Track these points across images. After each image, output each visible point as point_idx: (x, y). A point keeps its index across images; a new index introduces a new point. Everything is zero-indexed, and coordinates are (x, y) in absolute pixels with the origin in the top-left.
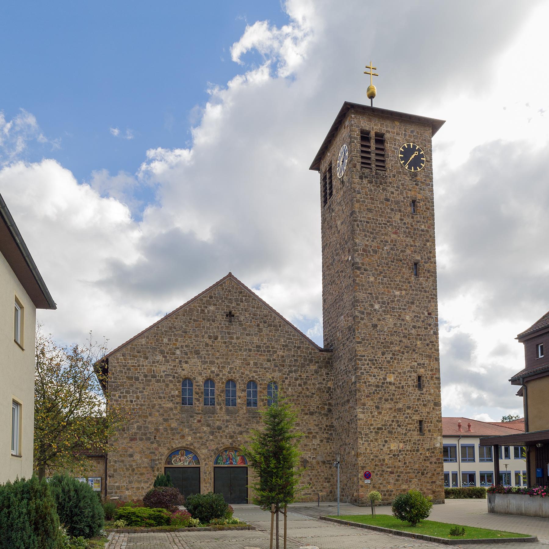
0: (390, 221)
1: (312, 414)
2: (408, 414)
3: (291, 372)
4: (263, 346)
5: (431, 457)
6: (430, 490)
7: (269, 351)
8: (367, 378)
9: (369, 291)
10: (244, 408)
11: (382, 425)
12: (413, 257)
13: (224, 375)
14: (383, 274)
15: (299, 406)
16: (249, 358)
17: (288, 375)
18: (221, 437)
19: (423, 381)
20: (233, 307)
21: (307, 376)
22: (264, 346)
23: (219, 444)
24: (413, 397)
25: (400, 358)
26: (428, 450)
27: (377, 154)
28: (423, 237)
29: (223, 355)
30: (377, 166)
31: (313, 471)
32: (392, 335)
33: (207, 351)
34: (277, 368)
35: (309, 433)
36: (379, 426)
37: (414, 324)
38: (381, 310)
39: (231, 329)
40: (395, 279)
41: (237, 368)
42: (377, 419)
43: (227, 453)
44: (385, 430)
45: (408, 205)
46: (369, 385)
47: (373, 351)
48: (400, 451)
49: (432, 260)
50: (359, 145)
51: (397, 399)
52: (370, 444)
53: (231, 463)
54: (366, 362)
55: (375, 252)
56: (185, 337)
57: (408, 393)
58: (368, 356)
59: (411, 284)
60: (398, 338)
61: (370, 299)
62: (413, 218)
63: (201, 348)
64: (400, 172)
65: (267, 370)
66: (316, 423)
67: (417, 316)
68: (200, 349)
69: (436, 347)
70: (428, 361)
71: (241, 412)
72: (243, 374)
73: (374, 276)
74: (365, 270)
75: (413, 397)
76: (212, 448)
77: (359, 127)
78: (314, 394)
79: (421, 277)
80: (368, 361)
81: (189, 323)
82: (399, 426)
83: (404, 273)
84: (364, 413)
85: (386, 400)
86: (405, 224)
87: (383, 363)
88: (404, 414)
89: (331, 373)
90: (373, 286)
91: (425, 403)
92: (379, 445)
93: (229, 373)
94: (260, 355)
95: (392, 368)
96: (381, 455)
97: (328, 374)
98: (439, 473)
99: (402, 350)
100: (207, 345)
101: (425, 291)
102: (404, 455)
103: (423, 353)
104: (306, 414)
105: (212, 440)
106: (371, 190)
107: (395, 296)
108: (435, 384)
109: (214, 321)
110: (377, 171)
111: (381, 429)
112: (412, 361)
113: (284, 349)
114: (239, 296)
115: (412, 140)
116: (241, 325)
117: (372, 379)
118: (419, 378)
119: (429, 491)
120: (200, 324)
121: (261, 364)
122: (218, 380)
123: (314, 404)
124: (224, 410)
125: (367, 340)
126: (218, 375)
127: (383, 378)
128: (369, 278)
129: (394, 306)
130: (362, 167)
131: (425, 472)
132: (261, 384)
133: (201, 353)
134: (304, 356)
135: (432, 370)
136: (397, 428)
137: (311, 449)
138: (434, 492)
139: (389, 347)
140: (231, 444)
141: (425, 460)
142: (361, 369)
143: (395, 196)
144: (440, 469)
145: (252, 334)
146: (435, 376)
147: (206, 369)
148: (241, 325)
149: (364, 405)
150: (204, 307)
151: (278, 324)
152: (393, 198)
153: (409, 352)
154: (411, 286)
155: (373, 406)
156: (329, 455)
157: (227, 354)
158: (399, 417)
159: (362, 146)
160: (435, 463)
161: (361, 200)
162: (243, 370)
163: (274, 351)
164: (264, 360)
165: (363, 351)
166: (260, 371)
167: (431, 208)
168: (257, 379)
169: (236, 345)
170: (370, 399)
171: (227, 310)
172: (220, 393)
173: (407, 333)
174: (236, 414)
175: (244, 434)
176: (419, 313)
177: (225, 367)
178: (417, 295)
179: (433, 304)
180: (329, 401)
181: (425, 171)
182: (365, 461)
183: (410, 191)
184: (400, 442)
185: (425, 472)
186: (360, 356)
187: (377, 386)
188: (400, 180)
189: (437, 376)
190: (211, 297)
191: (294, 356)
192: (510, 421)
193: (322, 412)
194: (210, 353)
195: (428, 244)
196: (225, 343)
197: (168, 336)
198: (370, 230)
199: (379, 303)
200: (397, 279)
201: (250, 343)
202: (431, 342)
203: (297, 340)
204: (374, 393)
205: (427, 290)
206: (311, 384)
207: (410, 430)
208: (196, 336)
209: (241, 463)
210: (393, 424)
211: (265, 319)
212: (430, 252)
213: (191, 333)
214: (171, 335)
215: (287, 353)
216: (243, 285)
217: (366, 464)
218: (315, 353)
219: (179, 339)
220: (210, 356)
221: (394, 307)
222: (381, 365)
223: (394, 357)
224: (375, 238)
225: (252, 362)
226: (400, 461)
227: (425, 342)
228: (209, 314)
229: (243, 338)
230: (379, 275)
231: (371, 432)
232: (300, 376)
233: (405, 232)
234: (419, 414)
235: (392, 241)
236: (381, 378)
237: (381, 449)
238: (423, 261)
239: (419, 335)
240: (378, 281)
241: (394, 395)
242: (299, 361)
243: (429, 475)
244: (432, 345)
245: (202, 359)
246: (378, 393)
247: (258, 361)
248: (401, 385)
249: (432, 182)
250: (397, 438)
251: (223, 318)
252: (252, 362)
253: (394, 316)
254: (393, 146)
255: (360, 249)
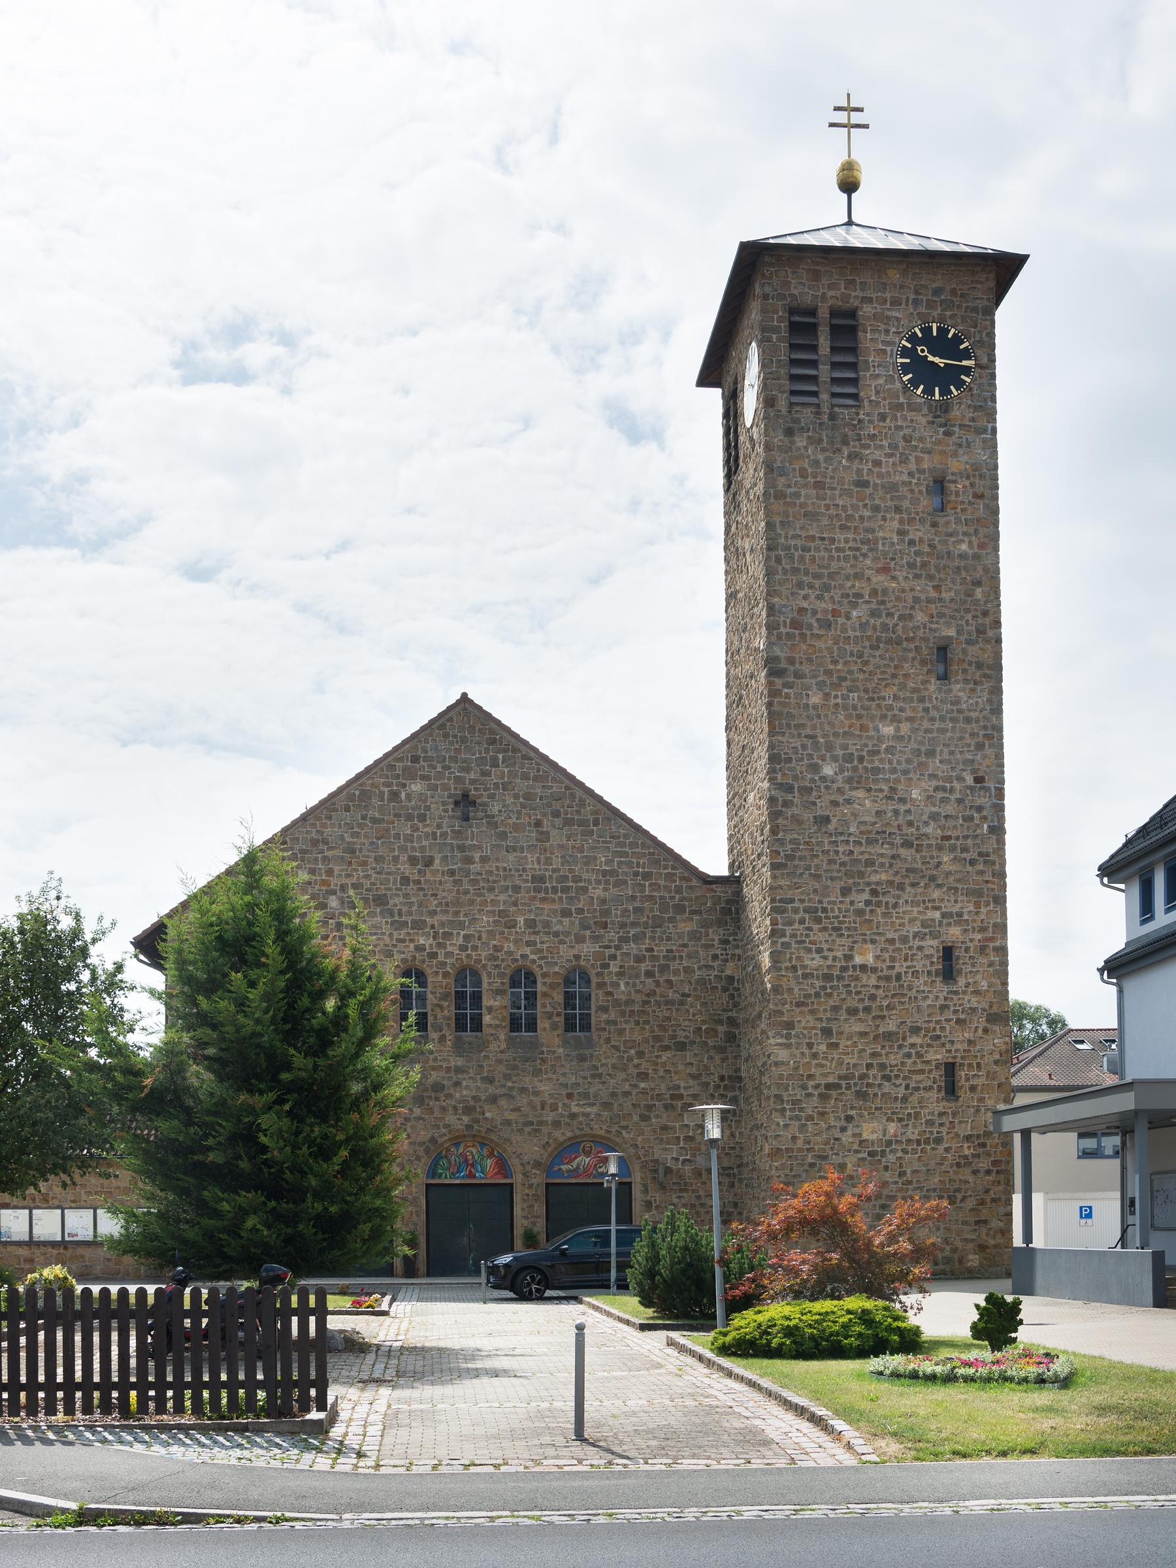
0: (869, 540)
1: (681, 1046)
2: (913, 1045)
3: (624, 940)
4: (551, 877)
5: (978, 1156)
6: (972, 1241)
7: (566, 890)
8: (798, 958)
9: (809, 731)
10: (502, 1037)
11: (840, 1078)
12: (935, 630)
13: (449, 955)
14: (848, 683)
15: (647, 1027)
16: (515, 908)
17: (618, 948)
18: (443, 1109)
19: (958, 958)
20: (473, 782)
21: (668, 951)
22: (554, 876)
23: (438, 1127)
24: (929, 1002)
25: (892, 901)
26: (968, 1138)
27: (814, 379)
28: (964, 574)
29: (447, 904)
30: (834, 395)
31: (684, 1194)
32: (870, 842)
33: (406, 896)
34: (588, 933)
35: (673, 1097)
36: (831, 1080)
37: (933, 809)
38: (840, 777)
39: (467, 839)
40: (882, 694)
41: (484, 936)
42: (825, 1062)
43: (461, 1150)
44: (848, 1087)
45: (920, 492)
46: (805, 976)
47: (817, 885)
48: (889, 1143)
49: (990, 633)
50: (784, 346)
51: (881, 1010)
52: (804, 1125)
53: (473, 1176)
54: (797, 917)
55: (827, 625)
56: (350, 863)
57: (913, 993)
58: (802, 901)
59: (927, 705)
60: (886, 850)
61: (810, 751)
62: (934, 525)
63: (390, 889)
64: (902, 403)
65: (561, 937)
66: (694, 1071)
67: (944, 789)
68: (388, 892)
69: (997, 867)
70: (971, 908)
71: (493, 1047)
72: (497, 949)
73: (821, 690)
74: (798, 675)
75: (929, 1002)
76: (420, 1139)
77: (783, 297)
78: (689, 996)
79: (957, 682)
80: (801, 914)
81: (360, 826)
82: (887, 1078)
83: (906, 676)
84: (788, 1046)
85: (852, 1012)
86: (912, 543)
87: (844, 917)
88: (900, 1047)
89: (735, 940)
90: (819, 716)
91: (962, 1017)
92: (829, 1128)
93: (463, 948)
94: (543, 900)
95: (872, 929)
96: (837, 1154)
97: (726, 942)
98: (1000, 1199)
99: (897, 880)
100: (405, 880)
101: (968, 720)
102: (900, 1154)
103: (960, 886)
104: (667, 1048)
105: (420, 1118)
106: (816, 463)
107: (880, 739)
108: (991, 965)
109: (422, 818)
110: (836, 409)
111: (836, 1086)
112: (927, 908)
113: (607, 882)
114: (487, 750)
115: (935, 313)
116: (493, 824)
117: (813, 959)
118: (948, 953)
119: (971, 1246)
120: (388, 830)
121: (547, 924)
122: (435, 969)
123: (687, 1023)
124: (449, 1043)
125: (801, 858)
126: (433, 955)
127: (845, 956)
128: (808, 695)
129: (877, 764)
130: (792, 404)
131: (959, 1196)
132: (544, 975)
133: (391, 902)
134: (662, 898)
135: (983, 929)
136: (880, 1085)
137: (678, 1138)
138: (982, 1248)
139: (861, 875)
140: (468, 1127)
141: (958, 1165)
142: (784, 935)
143: (883, 470)
144: (1001, 1188)
145: (522, 847)
146: (991, 945)
147: (403, 941)
148: (493, 824)
149: (790, 1025)
150: (397, 786)
151: (591, 818)
152: (880, 475)
153: (918, 884)
154: (926, 710)
155: (813, 1028)
156: (727, 1154)
157: (457, 902)
158: (886, 1055)
159: (793, 347)
160: (988, 1172)
161: (789, 491)
162: (499, 941)
163: (578, 889)
164: (554, 912)
165: (790, 887)
166: (542, 942)
167: (988, 493)
168: (534, 961)
169: (479, 877)
170: (806, 1009)
171: (456, 789)
172: (441, 999)
173: (912, 835)
174: (480, 1052)
175: (502, 1102)
176: (949, 779)
177: (452, 934)
178: (943, 731)
179: (989, 751)
180: (730, 1014)
181: (972, 395)
182: (792, 1169)
183: (929, 452)
184: (890, 1120)
185: (959, 1196)
186: (779, 902)
187: (827, 977)
188: (899, 428)
189: (998, 944)
190: (415, 759)
191: (633, 898)
192: (149, 1211)
193: (711, 1042)
194: (414, 899)
195: (979, 592)
196: (452, 873)
197: (309, 862)
198: (813, 569)
199: (835, 759)
200: (888, 693)
201: (518, 870)
202: (980, 854)
203: (639, 856)
204: (817, 995)
205: (973, 715)
206: (679, 970)
207: (917, 1089)
208: (379, 859)
209: (496, 1174)
210: (871, 1073)
211: (557, 805)
212: (985, 614)
213: (365, 852)
214: (316, 859)
215: (614, 891)
216: (498, 722)
217: (795, 1176)
218: (691, 888)
219: (336, 869)
220: (415, 908)
221: (878, 768)
222: (840, 922)
223: (874, 899)
224: (826, 588)
225: (521, 920)
226: (886, 1168)
227: (964, 855)
228: (410, 801)
229: (497, 860)
230: (836, 686)
231: (809, 1095)
232: (651, 950)
233: (911, 565)
234: (943, 1045)
235: (874, 593)
236: (839, 954)
237: (836, 1139)
238: (962, 638)
239: (948, 838)
240: (833, 701)
241: (873, 997)
242: (647, 912)
243: (971, 1203)
244: (985, 862)
245: (392, 916)
246: (830, 995)
247: (537, 915)
248: (894, 973)
249: (995, 420)
250: (881, 1108)
251: (446, 811)
252: (521, 920)
253: (876, 790)
254: (883, 337)
255: (785, 622)
